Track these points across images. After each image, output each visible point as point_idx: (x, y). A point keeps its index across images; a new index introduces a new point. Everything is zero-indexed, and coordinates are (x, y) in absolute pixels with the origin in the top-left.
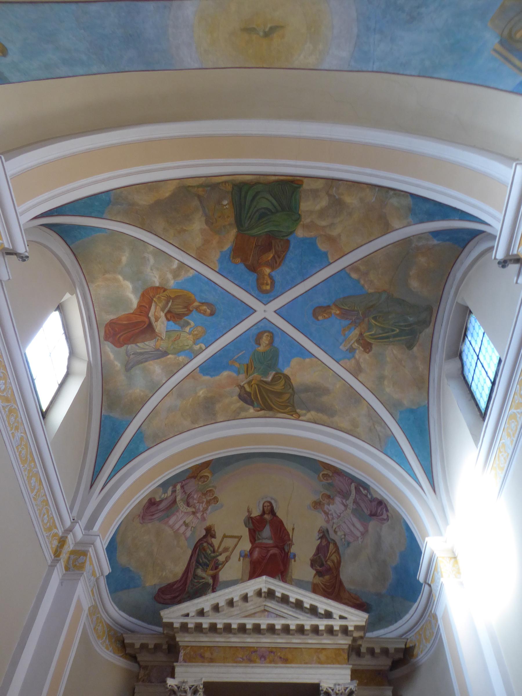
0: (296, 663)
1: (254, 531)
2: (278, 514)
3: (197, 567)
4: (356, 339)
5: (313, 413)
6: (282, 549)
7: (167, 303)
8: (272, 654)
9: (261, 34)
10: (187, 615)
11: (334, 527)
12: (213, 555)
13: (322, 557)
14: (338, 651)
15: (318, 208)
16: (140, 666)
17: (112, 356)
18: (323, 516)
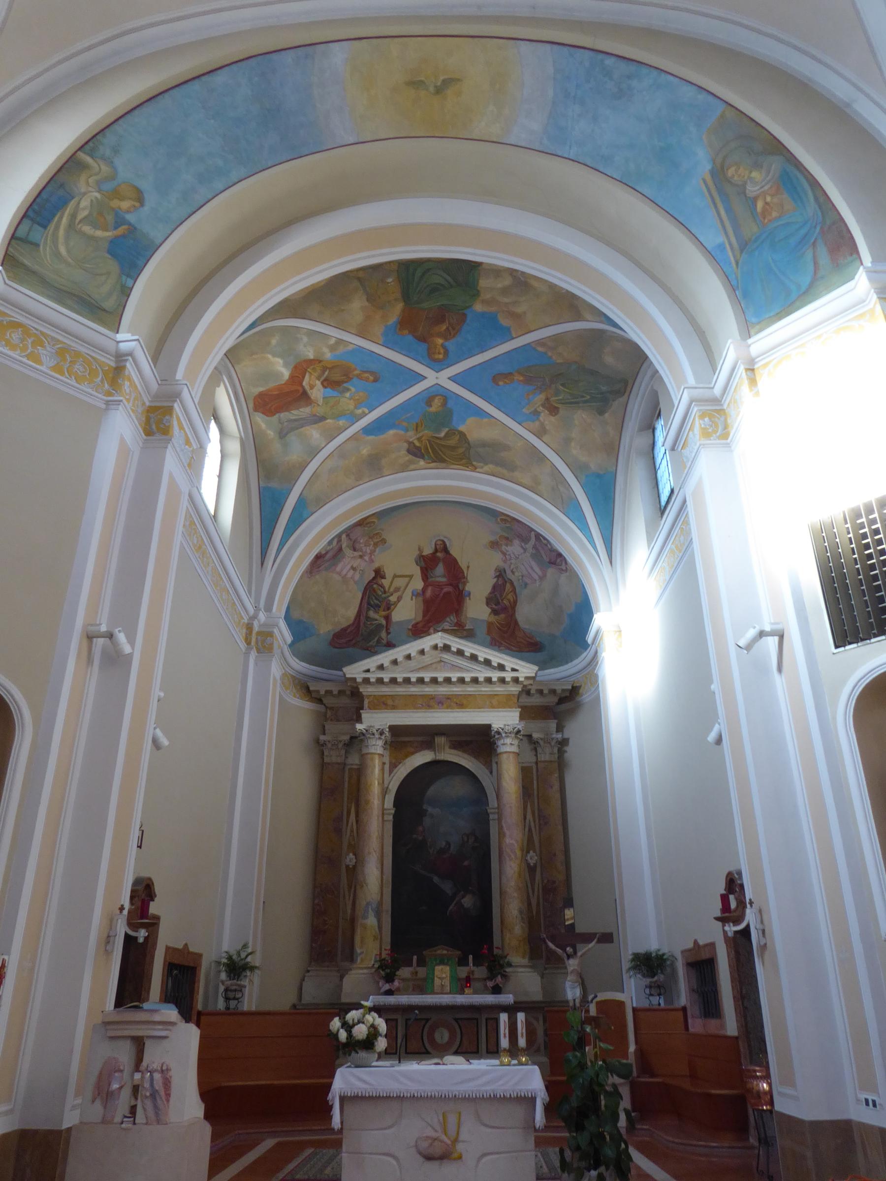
0: (471, 708)
1: (426, 569)
2: (452, 552)
3: (368, 609)
4: (541, 403)
5: (491, 466)
6: (456, 587)
7: (323, 373)
8: (449, 700)
9: (432, 89)
10: (368, 671)
11: (512, 567)
12: (384, 596)
13: (498, 596)
14: (509, 696)
15: (500, 285)
16: (327, 707)
17: (263, 426)
18: (500, 556)
